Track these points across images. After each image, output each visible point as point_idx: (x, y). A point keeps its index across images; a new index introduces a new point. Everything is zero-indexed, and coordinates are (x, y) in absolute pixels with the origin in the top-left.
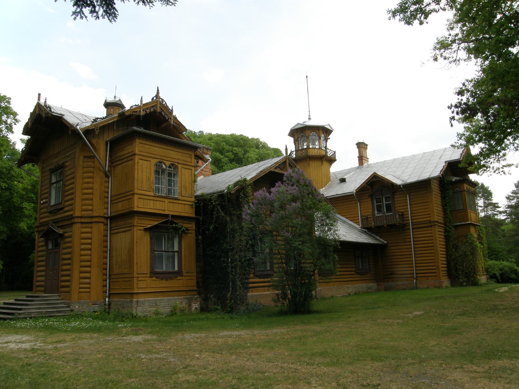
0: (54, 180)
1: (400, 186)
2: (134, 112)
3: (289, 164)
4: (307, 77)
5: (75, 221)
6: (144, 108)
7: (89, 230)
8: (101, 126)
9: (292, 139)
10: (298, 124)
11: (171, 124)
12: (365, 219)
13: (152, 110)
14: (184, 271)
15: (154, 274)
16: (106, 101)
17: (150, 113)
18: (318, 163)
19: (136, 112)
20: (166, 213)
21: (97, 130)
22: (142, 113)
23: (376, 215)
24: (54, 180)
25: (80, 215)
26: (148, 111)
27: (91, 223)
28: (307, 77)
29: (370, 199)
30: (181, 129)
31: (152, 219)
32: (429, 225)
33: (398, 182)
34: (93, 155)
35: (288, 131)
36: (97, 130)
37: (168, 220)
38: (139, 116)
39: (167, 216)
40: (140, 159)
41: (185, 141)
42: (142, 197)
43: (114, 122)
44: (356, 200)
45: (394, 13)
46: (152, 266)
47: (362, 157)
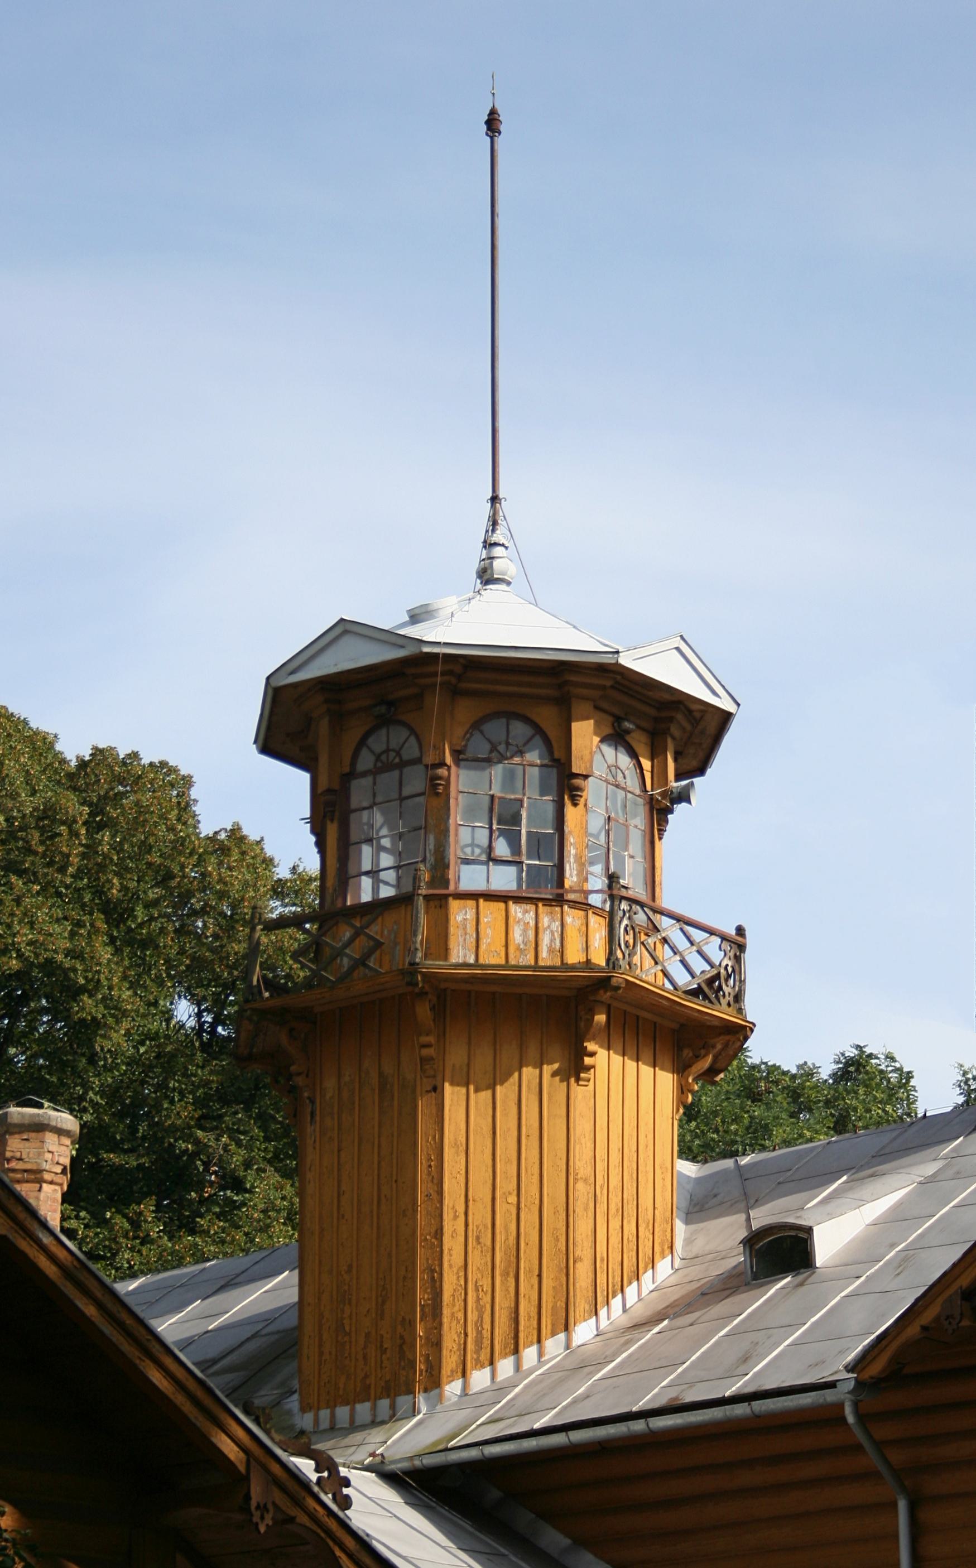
4: (492, 124)
10: (344, 629)
28: (492, 124)
35: (282, 634)
44: (870, 1475)
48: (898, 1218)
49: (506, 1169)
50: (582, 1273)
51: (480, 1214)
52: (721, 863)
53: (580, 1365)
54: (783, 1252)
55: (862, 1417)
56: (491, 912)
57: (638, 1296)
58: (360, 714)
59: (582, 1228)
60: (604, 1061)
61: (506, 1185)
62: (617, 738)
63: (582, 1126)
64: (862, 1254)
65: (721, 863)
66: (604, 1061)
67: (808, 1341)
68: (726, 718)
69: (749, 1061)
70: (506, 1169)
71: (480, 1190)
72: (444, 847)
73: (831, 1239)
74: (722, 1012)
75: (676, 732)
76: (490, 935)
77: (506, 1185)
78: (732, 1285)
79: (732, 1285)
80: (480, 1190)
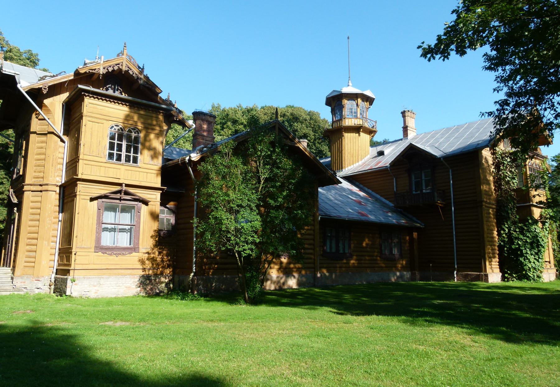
1: (440, 158)
2: (92, 70)
3: (279, 128)
4: (348, 38)
5: (49, 189)
6: (104, 66)
7: (39, 199)
9: (329, 109)
10: (334, 91)
13: (116, 68)
14: (140, 247)
15: (100, 248)
18: (354, 135)
19: (95, 69)
21: (45, 89)
22: (102, 71)
23: (414, 193)
25: (31, 183)
26: (110, 69)
27: (41, 191)
32: (40, 188)
33: (437, 153)
36: (45, 89)
39: (120, 185)
40: (89, 121)
42: (89, 162)
43: (66, 82)
46: (98, 240)
47: (407, 127)
49: (352, 146)
50: (360, 156)
51: (349, 151)
52: (372, 115)
53: (360, 166)
54: (381, 153)
55: (391, 170)
56: (350, 120)
57: (366, 159)
58: (335, 101)
59: (360, 152)
60: (362, 134)
61: (352, 148)
62: (363, 101)
63: (360, 141)
65: (372, 115)
66: (362, 134)
67: (386, 161)
68: (374, 99)
69: (487, 49)
70: (352, 146)
71: (349, 148)
72: (191, 380)
73: (386, 153)
74: (374, 129)
75: (370, 100)
77: (352, 148)
79: (376, 157)
80: (349, 148)
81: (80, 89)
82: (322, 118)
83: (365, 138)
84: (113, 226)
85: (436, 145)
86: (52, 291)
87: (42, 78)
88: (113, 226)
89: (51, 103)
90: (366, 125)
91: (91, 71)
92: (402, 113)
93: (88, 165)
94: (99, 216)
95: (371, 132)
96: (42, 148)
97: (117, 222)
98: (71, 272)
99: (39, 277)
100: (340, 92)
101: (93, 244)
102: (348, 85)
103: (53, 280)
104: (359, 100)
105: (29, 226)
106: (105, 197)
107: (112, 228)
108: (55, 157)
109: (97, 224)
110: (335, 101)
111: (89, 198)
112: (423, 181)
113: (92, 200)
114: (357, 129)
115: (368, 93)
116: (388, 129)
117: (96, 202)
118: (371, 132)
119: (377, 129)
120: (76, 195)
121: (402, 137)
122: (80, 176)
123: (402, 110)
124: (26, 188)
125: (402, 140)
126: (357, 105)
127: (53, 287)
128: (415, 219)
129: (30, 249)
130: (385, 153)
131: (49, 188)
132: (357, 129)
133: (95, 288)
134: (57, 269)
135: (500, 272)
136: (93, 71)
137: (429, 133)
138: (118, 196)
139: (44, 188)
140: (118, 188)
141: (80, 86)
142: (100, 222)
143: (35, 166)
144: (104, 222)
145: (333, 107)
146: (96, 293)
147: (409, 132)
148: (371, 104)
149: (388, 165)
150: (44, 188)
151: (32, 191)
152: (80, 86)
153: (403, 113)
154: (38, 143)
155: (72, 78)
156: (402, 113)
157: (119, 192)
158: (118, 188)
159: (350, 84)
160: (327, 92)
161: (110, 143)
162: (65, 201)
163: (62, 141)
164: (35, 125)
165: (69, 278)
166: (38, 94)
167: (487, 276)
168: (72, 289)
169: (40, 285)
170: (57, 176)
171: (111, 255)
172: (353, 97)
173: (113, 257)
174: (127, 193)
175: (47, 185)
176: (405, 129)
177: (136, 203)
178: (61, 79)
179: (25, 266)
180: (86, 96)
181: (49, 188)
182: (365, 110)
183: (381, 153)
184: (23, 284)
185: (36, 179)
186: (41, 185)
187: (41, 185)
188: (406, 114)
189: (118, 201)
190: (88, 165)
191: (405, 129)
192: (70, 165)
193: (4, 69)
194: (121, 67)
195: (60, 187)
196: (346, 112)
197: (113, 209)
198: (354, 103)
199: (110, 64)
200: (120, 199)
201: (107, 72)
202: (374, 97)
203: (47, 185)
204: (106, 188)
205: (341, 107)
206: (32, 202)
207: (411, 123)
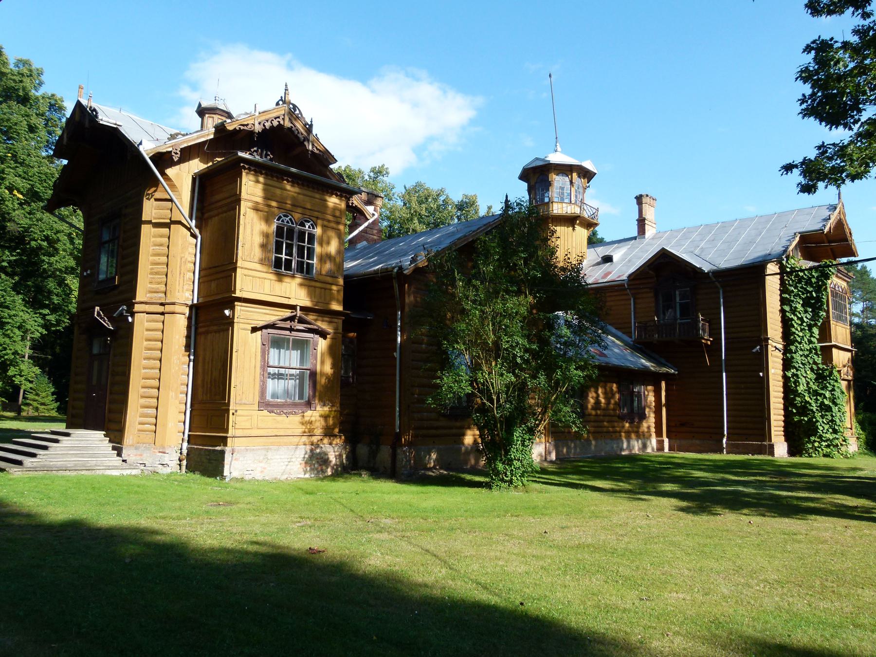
0: (106, 237)
2: (243, 125)
4: (550, 76)
5: (177, 311)
8: (183, 146)
9: (525, 185)
10: (537, 159)
11: (308, 150)
12: (643, 327)
13: (275, 123)
15: (265, 405)
16: (200, 105)
17: (272, 127)
19: (247, 125)
20: (292, 302)
21: (176, 153)
22: (258, 128)
24: (106, 237)
25: (142, 300)
26: (268, 125)
27: (163, 314)
28: (550, 76)
29: (652, 295)
30: (327, 159)
31: (267, 311)
32: (161, 309)
34: (168, 197)
35: (519, 172)
37: (296, 316)
38: (252, 133)
39: (293, 307)
41: (334, 181)
42: (250, 273)
43: (204, 143)
45: (804, 52)
48: (625, 254)
54: (608, 259)
58: (538, 176)
60: (577, 228)
62: (579, 177)
64: (622, 259)
65: (595, 200)
66: (577, 228)
75: (587, 175)
76: (557, 209)
78: (598, 264)
79: (598, 264)
81: (241, 158)
82: (45, 90)
83: (582, 233)
84: (276, 370)
85: (696, 252)
86: (184, 468)
87: (173, 137)
88: (276, 370)
89: (177, 174)
90: (586, 215)
91: (242, 128)
92: (636, 198)
93: (249, 276)
94: (264, 354)
95: (589, 224)
96: (161, 245)
97: (282, 365)
98: (229, 440)
99: (164, 448)
100: (543, 160)
101: (257, 399)
102: (556, 151)
103: (185, 451)
104: (575, 175)
105: (144, 368)
106: (272, 326)
107: (275, 374)
108: (183, 260)
109: (261, 368)
110: (538, 176)
111: (249, 327)
112: (678, 305)
113: (254, 330)
114: (571, 221)
115: (588, 165)
116: (615, 221)
117: (259, 333)
118: (589, 224)
119: (599, 221)
120: (233, 323)
121: (635, 234)
122: (238, 294)
123: (638, 194)
124: (137, 308)
125: (635, 238)
126: (571, 182)
127: (184, 463)
128: (663, 360)
129: (147, 404)
130: (615, 259)
131: (177, 308)
132: (571, 221)
133: (262, 465)
134: (189, 435)
135: (786, 441)
136: (245, 128)
137: (678, 231)
138: (287, 324)
139: (168, 308)
140: (287, 313)
141: (240, 154)
142: (265, 365)
143: (151, 274)
144: (271, 364)
145: (532, 183)
146: (262, 472)
147: (647, 227)
148: (641, 196)
149: (625, 277)
150: (168, 308)
151: (148, 313)
152: (240, 154)
153: (639, 199)
154: (154, 236)
155: (212, 137)
156: (636, 198)
157: (291, 319)
158: (287, 313)
159: (559, 149)
160: (525, 160)
161: (277, 241)
162: (200, 330)
163: (194, 236)
164: (150, 209)
165: (228, 449)
166: (163, 160)
167: (772, 447)
168: (233, 467)
169: (166, 459)
170: (187, 290)
171: (279, 414)
172: (566, 170)
173: (283, 418)
174: (301, 321)
175: (173, 304)
176: (641, 223)
177: (311, 335)
178: (198, 138)
179: (139, 430)
180: (245, 169)
181: (177, 308)
182: (581, 190)
183: (608, 259)
184: (138, 458)
185: (156, 295)
186: (162, 304)
187: (162, 304)
188: (644, 200)
189: (288, 332)
190: (249, 276)
191: (641, 223)
192: (205, 276)
193: (100, 117)
194: (282, 122)
195: (191, 307)
196: (554, 192)
197: (278, 343)
198: (567, 179)
199: (267, 117)
200: (291, 330)
201: (263, 130)
202: (595, 171)
203: (173, 304)
204: (272, 312)
205: (548, 185)
206: (148, 330)
207: (649, 213)
